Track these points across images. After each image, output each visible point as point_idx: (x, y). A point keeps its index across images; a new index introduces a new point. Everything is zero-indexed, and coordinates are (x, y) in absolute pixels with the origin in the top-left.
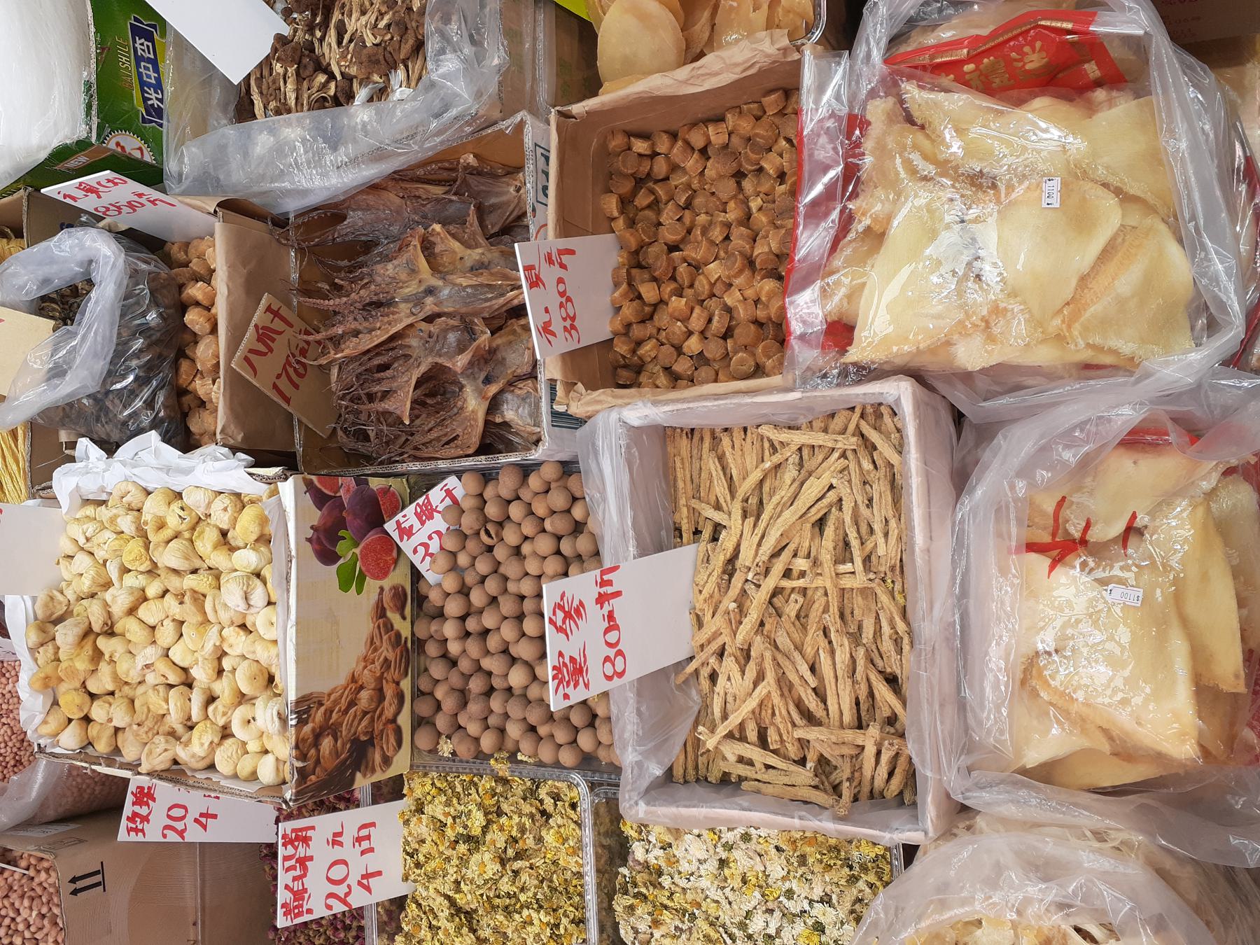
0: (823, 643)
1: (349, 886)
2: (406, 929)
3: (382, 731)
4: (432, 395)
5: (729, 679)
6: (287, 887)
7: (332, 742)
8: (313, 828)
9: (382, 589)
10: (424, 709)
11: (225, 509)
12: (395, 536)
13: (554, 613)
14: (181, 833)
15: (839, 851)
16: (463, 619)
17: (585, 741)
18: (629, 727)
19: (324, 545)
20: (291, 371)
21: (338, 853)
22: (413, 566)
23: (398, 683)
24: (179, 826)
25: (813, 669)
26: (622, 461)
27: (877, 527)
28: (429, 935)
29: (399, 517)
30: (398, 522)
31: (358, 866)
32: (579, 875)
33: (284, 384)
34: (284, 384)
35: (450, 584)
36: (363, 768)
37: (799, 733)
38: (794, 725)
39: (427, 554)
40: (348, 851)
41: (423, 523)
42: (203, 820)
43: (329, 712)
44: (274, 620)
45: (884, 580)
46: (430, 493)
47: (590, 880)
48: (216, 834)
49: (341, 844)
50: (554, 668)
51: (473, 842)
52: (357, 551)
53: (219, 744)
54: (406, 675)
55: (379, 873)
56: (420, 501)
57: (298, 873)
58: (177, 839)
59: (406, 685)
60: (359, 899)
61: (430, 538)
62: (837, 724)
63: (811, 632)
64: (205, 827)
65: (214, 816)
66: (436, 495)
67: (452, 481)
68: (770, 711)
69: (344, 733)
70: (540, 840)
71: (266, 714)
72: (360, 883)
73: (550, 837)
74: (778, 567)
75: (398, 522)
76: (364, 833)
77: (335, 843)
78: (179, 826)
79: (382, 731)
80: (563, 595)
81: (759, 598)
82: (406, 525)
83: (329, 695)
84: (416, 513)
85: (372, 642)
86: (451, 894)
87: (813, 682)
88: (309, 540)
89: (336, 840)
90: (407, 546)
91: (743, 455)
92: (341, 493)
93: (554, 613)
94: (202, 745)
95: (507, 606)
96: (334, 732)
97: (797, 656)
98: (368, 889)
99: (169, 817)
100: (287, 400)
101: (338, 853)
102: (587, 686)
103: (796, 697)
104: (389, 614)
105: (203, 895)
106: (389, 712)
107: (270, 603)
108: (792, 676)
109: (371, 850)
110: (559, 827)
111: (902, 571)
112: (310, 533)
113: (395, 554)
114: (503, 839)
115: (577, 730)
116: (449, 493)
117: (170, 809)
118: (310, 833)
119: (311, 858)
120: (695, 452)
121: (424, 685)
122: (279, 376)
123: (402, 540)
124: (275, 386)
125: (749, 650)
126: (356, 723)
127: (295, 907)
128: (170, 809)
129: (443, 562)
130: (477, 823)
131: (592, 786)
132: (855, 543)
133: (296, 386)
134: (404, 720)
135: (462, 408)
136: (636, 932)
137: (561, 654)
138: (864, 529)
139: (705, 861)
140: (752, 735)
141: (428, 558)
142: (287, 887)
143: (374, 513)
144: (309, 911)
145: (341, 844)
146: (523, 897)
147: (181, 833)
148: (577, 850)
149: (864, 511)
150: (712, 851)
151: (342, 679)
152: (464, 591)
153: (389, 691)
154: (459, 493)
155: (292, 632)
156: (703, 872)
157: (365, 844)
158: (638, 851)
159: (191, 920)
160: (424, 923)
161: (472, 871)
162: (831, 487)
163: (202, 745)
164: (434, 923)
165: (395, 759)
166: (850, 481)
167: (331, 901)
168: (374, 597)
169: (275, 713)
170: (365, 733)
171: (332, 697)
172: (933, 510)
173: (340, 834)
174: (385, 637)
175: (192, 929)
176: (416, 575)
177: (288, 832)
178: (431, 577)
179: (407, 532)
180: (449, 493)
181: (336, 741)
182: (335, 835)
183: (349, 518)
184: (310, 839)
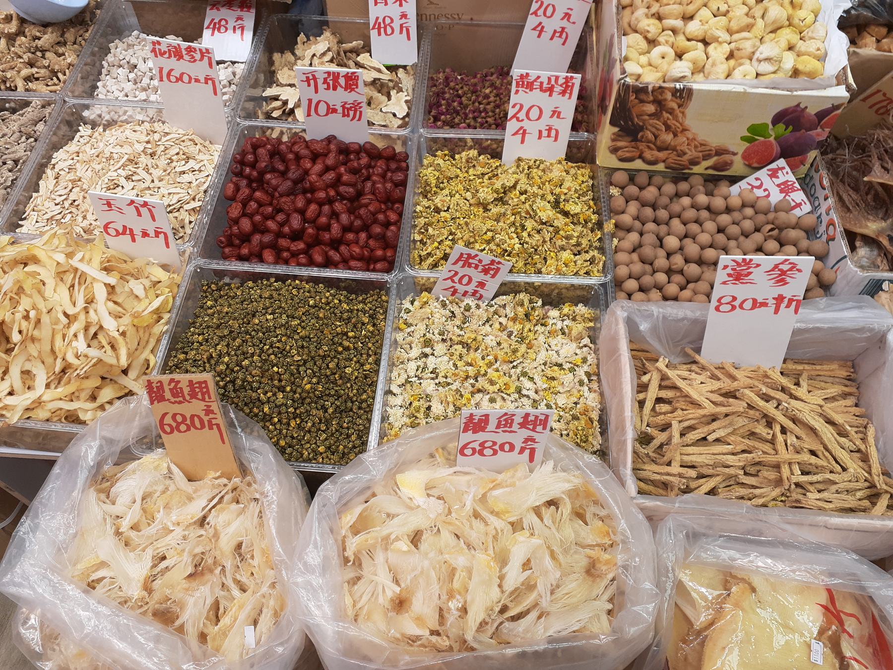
0: (739, 448)
1: (522, 120)
2: (481, 158)
3: (638, 148)
4: (876, 197)
5: (702, 383)
6: (539, 77)
7: (649, 113)
8: (570, 98)
9: (735, 154)
10: (642, 179)
11: (818, 49)
12: (773, 166)
13: (790, 263)
14: (535, 13)
15: (585, 442)
16: (708, 208)
17: (632, 284)
18: (675, 311)
19: (791, 117)
20: (885, 103)
21: (547, 113)
22: (741, 178)
23: (664, 161)
24: (540, 12)
25: (717, 440)
26: (861, 325)
27: (825, 495)
28: (479, 173)
29: (788, 169)
30: (784, 168)
31: (532, 127)
32: (540, 272)
33: (879, 97)
34: (879, 97)
35: (735, 201)
36: (620, 133)
37: (675, 424)
38: (680, 422)
39: (753, 187)
40: (546, 120)
41: (778, 186)
42: (539, 28)
43: (671, 112)
44: (747, 77)
45: (783, 495)
46: (801, 192)
47: (535, 279)
48: (528, 35)
49: (552, 117)
50: (751, 260)
51: (556, 204)
52: (772, 139)
53: (646, 38)
54: (666, 168)
55: (522, 142)
56: (797, 185)
57: (545, 85)
58: (532, 10)
59: (661, 167)
60: (512, 126)
61: (765, 190)
62: (684, 452)
63: (746, 441)
64: (534, 29)
65: (539, 36)
66: (799, 196)
67: (807, 208)
68: (684, 407)
69: (651, 121)
70: (563, 248)
71: (681, 68)
72: (522, 128)
73: (566, 255)
74: (789, 424)
75: (784, 168)
76: (553, 133)
77: (554, 112)
78: (540, 12)
79: (638, 148)
80: (799, 271)
81: (770, 408)
82: (780, 174)
83: (683, 113)
84: (788, 181)
85: (702, 145)
86: (518, 187)
87: (711, 438)
88: (798, 105)
89: (556, 113)
90: (763, 174)
91: (843, 412)
92: (819, 130)
93: (790, 263)
94: (649, 25)
95: (721, 238)
96: (656, 115)
97: (730, 430)
98: (516, 133)
99: (549, 5)
100: (864, 100)
101: (547, 113)
102: (724, 283)
103: (697, 426)
104: (715, 158)
105: (486, 26)
106: (648, 155)
107: (758, 75)
108: (715, 425)
109: (540, 138)
110: (575, 262)
111: (797, 507)
112: (802, 106)
113: (755, 165)
114: (559, 225)
115: (638, 279)
116: (799, 205)
117: (553, 6)
118: (567, 95)
119: (550, 95)
120: (837, 380)
121: (658, 179)
122: (884, 95)
123: (768, 170)
124: (879, 91)
125: (735, 397)
126: (654, 130)
127: (523, 83)
128: (553, 6)
129: (749, 197)
130: (573, 208)
131: (604, 285)
132: (815, 478)
133: (871, 107)
134: (638, 164)
135: (868, 219)
136: (504, 306)
137: (758, 265)
138: (820, 487)
139: (558, 355)
140: (664, 394)
141: (750, 187)
142: (539, 77)
143: (791, 152)
144: (517, 92)
145: (552, 117)
146: (525, 234)
147: (535, 13)
148: (559, 272)
149: (834, 488)
150: (567, 360)
151: (688, 122)
152: (728, 210)
153: (662, 155)
154: (797, 212)
155: (740, 89)
156: (550, 352)
157: (545, 133)
158: (554, 313)
159: (475, 17)
160: (486, 170)
161: (540, 203)
162: (844, 469)
163: (649, 25)
164: (486, 177)
165: (614, 156)
166: (850, 481)
167: (518, 107)
168: (732, 149)
169: (686, 74)
170: (642, 137)
171: (680, 115)
172: (853, 533)
173: (558, 117)
174: (701, 154)
175: (470, 17)
176: (734, 180)
177: (574, 81)
178: (735, 189)
179: (774, 174)
180: (799, 205)
181: (649, 115)
182: (559, 113)
183: (798, 134)
184: (563, 96)
